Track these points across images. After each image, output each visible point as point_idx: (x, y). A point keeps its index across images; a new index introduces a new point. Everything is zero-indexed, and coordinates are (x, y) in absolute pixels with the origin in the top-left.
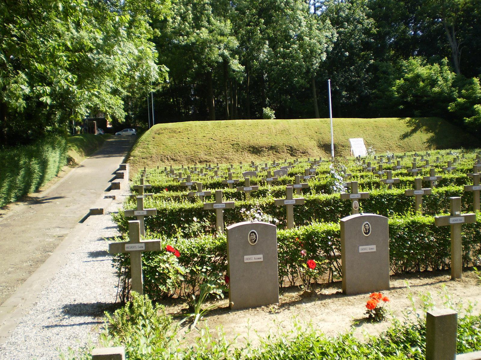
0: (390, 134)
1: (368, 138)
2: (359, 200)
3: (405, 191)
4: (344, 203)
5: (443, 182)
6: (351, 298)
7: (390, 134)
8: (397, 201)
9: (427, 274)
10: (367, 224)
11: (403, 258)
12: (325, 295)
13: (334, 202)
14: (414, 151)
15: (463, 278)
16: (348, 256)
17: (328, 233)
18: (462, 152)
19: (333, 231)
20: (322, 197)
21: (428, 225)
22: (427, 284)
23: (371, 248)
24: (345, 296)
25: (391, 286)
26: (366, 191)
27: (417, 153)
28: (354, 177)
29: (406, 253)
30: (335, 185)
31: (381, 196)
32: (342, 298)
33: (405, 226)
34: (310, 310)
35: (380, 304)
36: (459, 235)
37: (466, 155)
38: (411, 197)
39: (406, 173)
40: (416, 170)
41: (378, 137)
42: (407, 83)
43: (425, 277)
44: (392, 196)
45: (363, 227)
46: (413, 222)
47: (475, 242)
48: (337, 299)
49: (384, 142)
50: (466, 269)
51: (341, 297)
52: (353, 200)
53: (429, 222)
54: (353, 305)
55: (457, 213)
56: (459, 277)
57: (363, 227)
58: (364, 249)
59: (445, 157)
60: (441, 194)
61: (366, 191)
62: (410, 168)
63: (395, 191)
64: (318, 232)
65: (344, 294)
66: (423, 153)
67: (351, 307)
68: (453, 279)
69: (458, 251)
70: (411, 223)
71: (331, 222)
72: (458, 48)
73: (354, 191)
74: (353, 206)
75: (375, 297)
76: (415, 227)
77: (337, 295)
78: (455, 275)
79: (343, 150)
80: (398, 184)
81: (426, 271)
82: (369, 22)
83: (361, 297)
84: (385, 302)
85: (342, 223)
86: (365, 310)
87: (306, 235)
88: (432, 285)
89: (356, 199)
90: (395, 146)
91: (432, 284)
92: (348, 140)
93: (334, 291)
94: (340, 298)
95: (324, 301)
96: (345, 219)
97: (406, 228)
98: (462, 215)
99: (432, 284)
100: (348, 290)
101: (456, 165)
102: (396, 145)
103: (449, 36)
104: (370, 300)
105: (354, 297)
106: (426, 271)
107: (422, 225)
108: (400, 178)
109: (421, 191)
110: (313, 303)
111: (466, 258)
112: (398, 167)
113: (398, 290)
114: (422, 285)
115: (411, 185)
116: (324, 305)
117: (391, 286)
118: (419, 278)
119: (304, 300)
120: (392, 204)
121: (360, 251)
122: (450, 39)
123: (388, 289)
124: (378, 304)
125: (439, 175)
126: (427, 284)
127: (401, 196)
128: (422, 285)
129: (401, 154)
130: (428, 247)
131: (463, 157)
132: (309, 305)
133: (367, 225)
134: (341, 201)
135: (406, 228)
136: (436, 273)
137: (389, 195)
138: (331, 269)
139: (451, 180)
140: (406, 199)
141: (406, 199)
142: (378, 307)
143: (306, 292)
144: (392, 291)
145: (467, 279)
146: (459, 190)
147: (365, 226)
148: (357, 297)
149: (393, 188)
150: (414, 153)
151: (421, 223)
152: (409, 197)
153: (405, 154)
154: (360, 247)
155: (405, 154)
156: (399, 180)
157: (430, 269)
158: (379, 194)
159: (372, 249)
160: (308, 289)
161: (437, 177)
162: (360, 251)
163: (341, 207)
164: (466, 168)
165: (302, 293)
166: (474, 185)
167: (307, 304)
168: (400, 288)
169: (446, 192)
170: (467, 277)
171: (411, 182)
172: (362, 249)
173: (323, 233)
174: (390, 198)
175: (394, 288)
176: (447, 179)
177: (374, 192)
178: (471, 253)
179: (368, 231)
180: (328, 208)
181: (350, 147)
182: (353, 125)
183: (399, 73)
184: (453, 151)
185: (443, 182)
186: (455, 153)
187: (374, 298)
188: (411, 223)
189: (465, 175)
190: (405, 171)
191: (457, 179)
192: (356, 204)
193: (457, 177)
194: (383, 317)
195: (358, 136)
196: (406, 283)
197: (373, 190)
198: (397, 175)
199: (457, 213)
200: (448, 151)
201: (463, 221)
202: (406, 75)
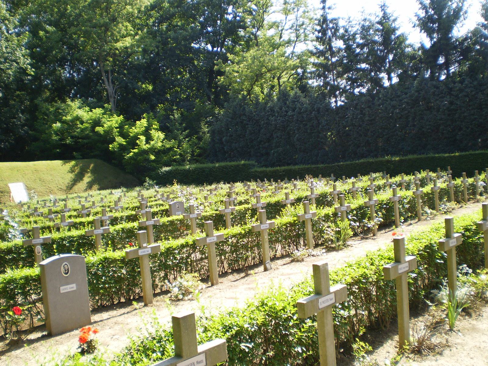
0: (50, 178)
1: (28, 183)
2: (42, 245)
3: (86, 232)
4: (25, 249)
5: (114, 221)
6: (58, 338)
7: (50, 178)
8: (78, 242)
9: (121, 305)
10: (66, 264)
11: (99, 293)
12: (31, 340)
13: (16, 249)
14: (76, 193)
15: (154, 303)
16: (51, 298)
17: (27, 279)
18: (123, 191)
19: (31, 276)
20: (2, 246)
21: (119, 260)
22: (124, 314)
23: (72, 287)
24: (51, 338)
25: (92, 321)
26: (47, 235)
27: (79, 195)
28: (27, 223)
29: (102, 288)
30: (10, 232)
31: (63, 239)
32: (49, 340)
33: (98, 263)
34: (21, 356)
35: (91, 336)
36: (147, 265)
37: (127, 194)
38: (91, 236)
39: (76, 215)
40: (85, 211)
41: (38, 181)
42: (66, 126)
43: (121, 308)
44: (72, 237)
45: (62, 267)
46: (106, 258)
47: (160, 270)
48: (45, 341)
49: (44, 186)
50: (155, 295)
51: (47, 339)
52: (35, 245)
53: (119, 256)
54: (62, 343)
55: (145, 245)
56: (151, 302)
57: (62, 267)
58: (64, 289)
59: (108, 197)
60: (118, 232)
61: (47, 235)
62: (78, 210)
63: (75, 233)
64: (16, 279)
65: (50, 335)
66: (85, 194)
67: (61, 346)
68: (146, 305)
69: (147, 279)
70: (103, 260)
71: (26, 267)
72: (114, 92)
73: (36, 236)
74: (36, 251)
75: (85, 331)
76: (107, 262)
77: (43, 338)
78: (147, 302)
79: (2, 196)
80: (75, 226)
81: (119, 302)
82: (25, 62)
83: (67, 336)
84: (95, 334)
85: (42, 266)
86: (77, 344)
87: (4, 283)
88: (129, 314)
89: (38, 244)
90: (56, 190)
91: (128, 313)
92: (6, 185)
93: (39, 335)
94: (47, 340)
95: (32, 346)
96: (44, 263)
97: (99, 264)
98: (148, 247)
99: (128, 313)
100: (54, 331)
101: (122, 204)
102: (57, 188)
103: (106, 80)
104: (82, 334)
105: (60, 337)
106: (119, 302)
107: (113, 260)
108: (73, 220)
109: (100, 231)
110: (22, 349)
111: (154, 286)
112: (65, 210)
113: (100, 323)
114: (120, 315)
115: (90, 225)
116: (34, 349)
117: (92, 321)
118: (115, 309)
119: (12, 348)
120: (73, 245)
121: (62, 292)
122: (106, 83)
123: (91, 323)
124: (89, 337)
125: (110, 214)
126: (124, 314)
127: (81, 237)
128: (120, 315)
129: (64, 197)
130: (119, 280)
131: (125, 195)
132: (18, 352)
133: (66, 266)
134: (22, 247)
135: (99, 264)
136: (128, 303)
137: (70, 237)
138: (31, 314)
139: (122, 218)
140: (86, 239)
141: (86, 239)
142: (89, 340)
143: (12, 340)
144: (95, 325)
145: (158, 304)
146: (134, 227)
147: (64, 266)
148: (63, 336)
149: (72, 230)
150: (75, 195)
151: (112, 259)
152: (89, 237)
153: (67, 196)
154: (61, 288)
155: (67, 196)
156: (73, 222)
157: (123, 300)
158: (60, 236)
159: (72, 288)
160: (13, 337)
161: (109, 216)
162: (62, 292)
163: (23, 254)
164: (131, 206)
165: (7, 342)
166: (95, 229)
167: (16, 351)
168: (101, 321)
169: (123, 229)
170: (157, 301)
171: (89, 223)
172: (209, 240)
173: (21, 279)
174: (71, 240)
175: (95, 322)
176: (118, 218)
177: (55, 235)
178: (157, 280)
179: (67, 271)
180: (10, 256)
181: (9, 192)
182: (12, 169)
183: (58, 116)
184: (114, 191)
185: (114, 221)
186: (117, 193)
187: (84, 332)
188: (103, 260)
189: (134, 213)
190: (75, 213)
191: (127, 216)
192: (38, 249)
193: (126, 215)
194: (95, 348)
195: (18, 181)
196: (105, 315)
197: (53, 234)
198: (70, 217)
199: (145, 245)
200: (109, 191)
201: (150, 252)
202: (64, 118)
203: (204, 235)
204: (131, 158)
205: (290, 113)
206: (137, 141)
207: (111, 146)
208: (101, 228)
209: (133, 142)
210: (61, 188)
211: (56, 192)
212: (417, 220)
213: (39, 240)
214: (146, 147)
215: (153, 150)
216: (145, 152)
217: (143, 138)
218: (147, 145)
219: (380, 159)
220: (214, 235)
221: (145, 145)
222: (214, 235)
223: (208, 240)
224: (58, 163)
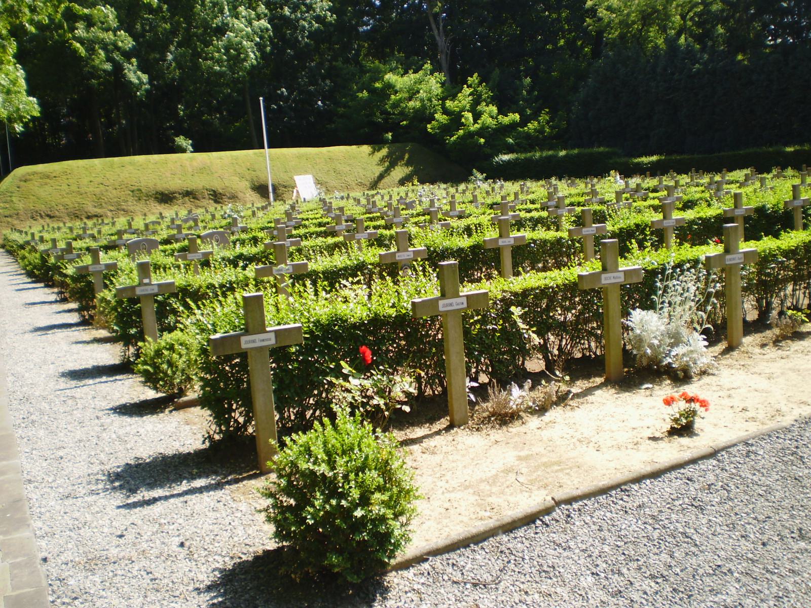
0: (348, 168)
1: (320, 175)
7: (348, 168)
92: (292, 178)
182: (299, 157)
203: (720, 249)
204: (455, 142)
205: (676, 77)
206: (463, 120)
207: (429, 126)
208: (594, 225)
209: (456, 119)
210: (361, 183)
211: (354, 187)
212: (443, 423)
213: (509, 239)
214: (474, 128)
215: (483, 131)
216: (470, 135)
217: (469, 116)
218: (476, 125)
219: (522, 156)
220: (461, 294)
221: (473, 125)
222: (620, 269)
223: (730, 259)
224: (366, 149)
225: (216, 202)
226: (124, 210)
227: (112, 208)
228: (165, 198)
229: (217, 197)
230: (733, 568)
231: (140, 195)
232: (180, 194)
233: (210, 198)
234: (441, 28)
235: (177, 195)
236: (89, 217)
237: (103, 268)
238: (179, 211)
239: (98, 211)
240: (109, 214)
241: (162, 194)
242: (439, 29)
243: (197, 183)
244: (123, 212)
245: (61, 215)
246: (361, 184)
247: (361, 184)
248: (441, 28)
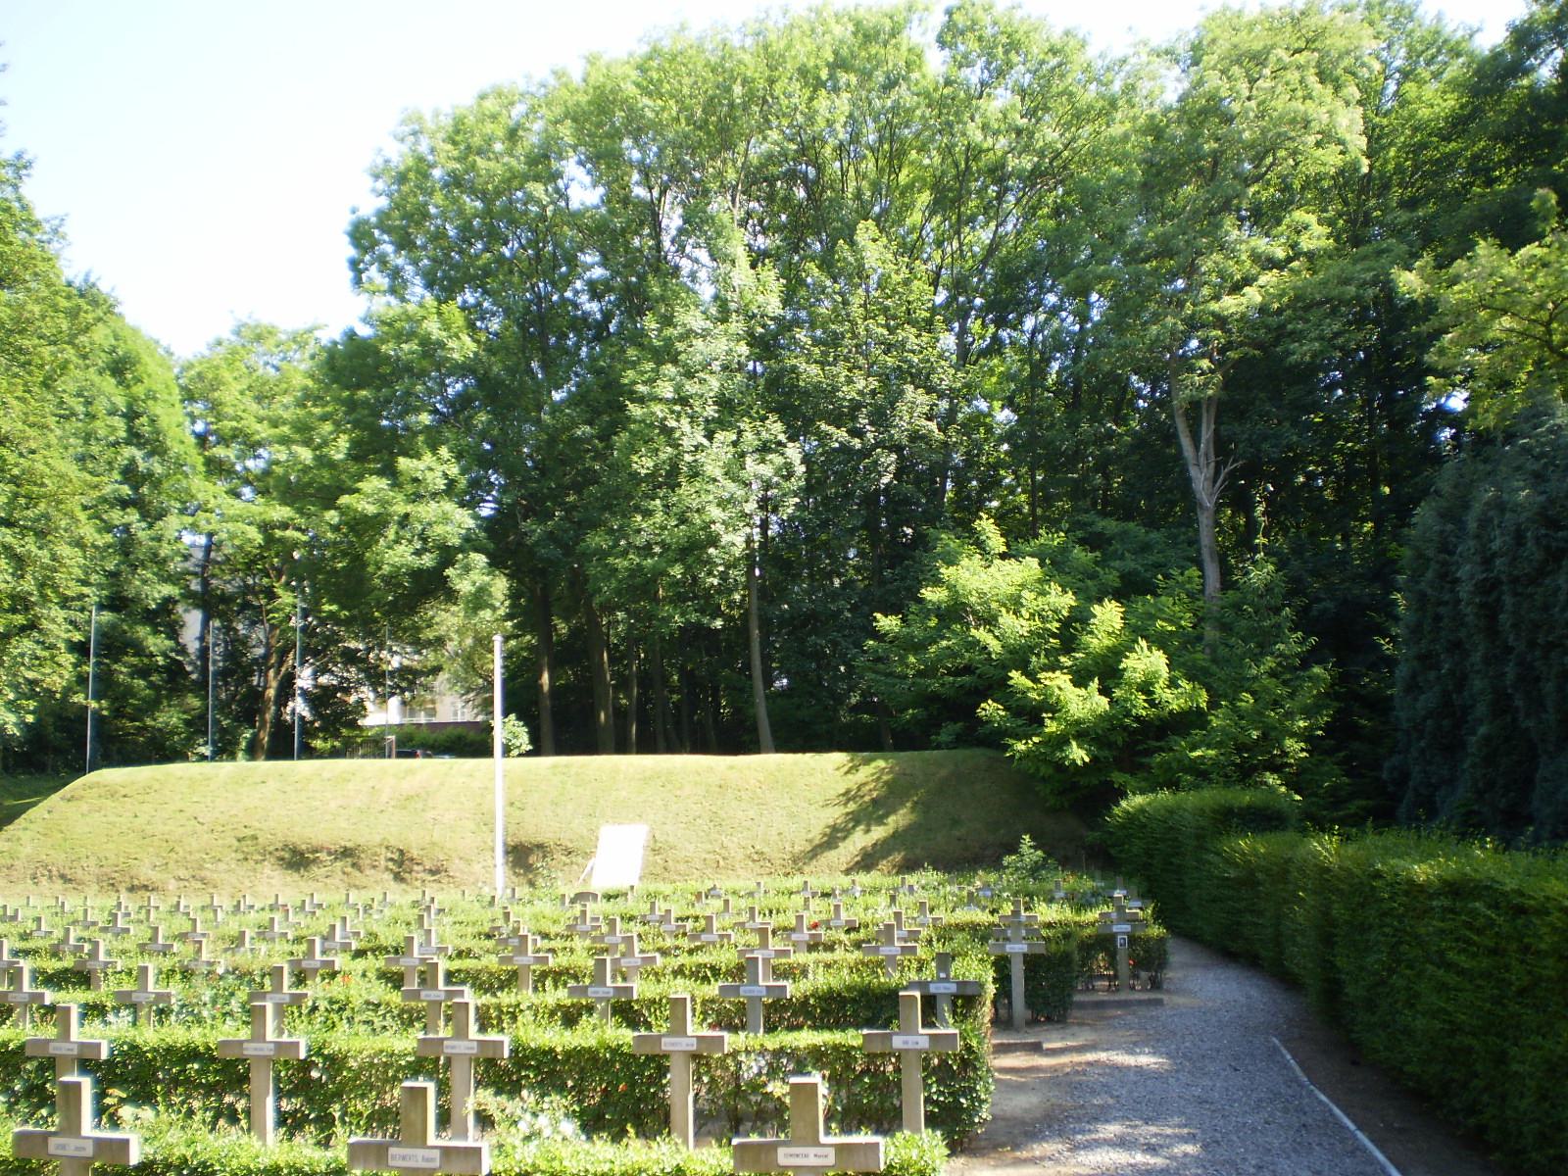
182: (555, 766)
225: (398, 878)
226: (203, 880)
227: (182, 873)
228: (297, 860)
229: (402, 865)
230: (785, 485)
231: (249, 848)
232: (330, 853)
233: (387, 869)
234: (1090, 1057)
235: (323, 856)
236: (132, 889)
237: (417, 962)
238: (326, 888)
239: (155, 876)
240: (172, 885)
241: (295, 851)
242: (1197, 447)
243: (375, 832)
244: (199, 885)
245: (87, 878)
246: (759, 858)
247: (759, 858)
248: (1090, 1057)
